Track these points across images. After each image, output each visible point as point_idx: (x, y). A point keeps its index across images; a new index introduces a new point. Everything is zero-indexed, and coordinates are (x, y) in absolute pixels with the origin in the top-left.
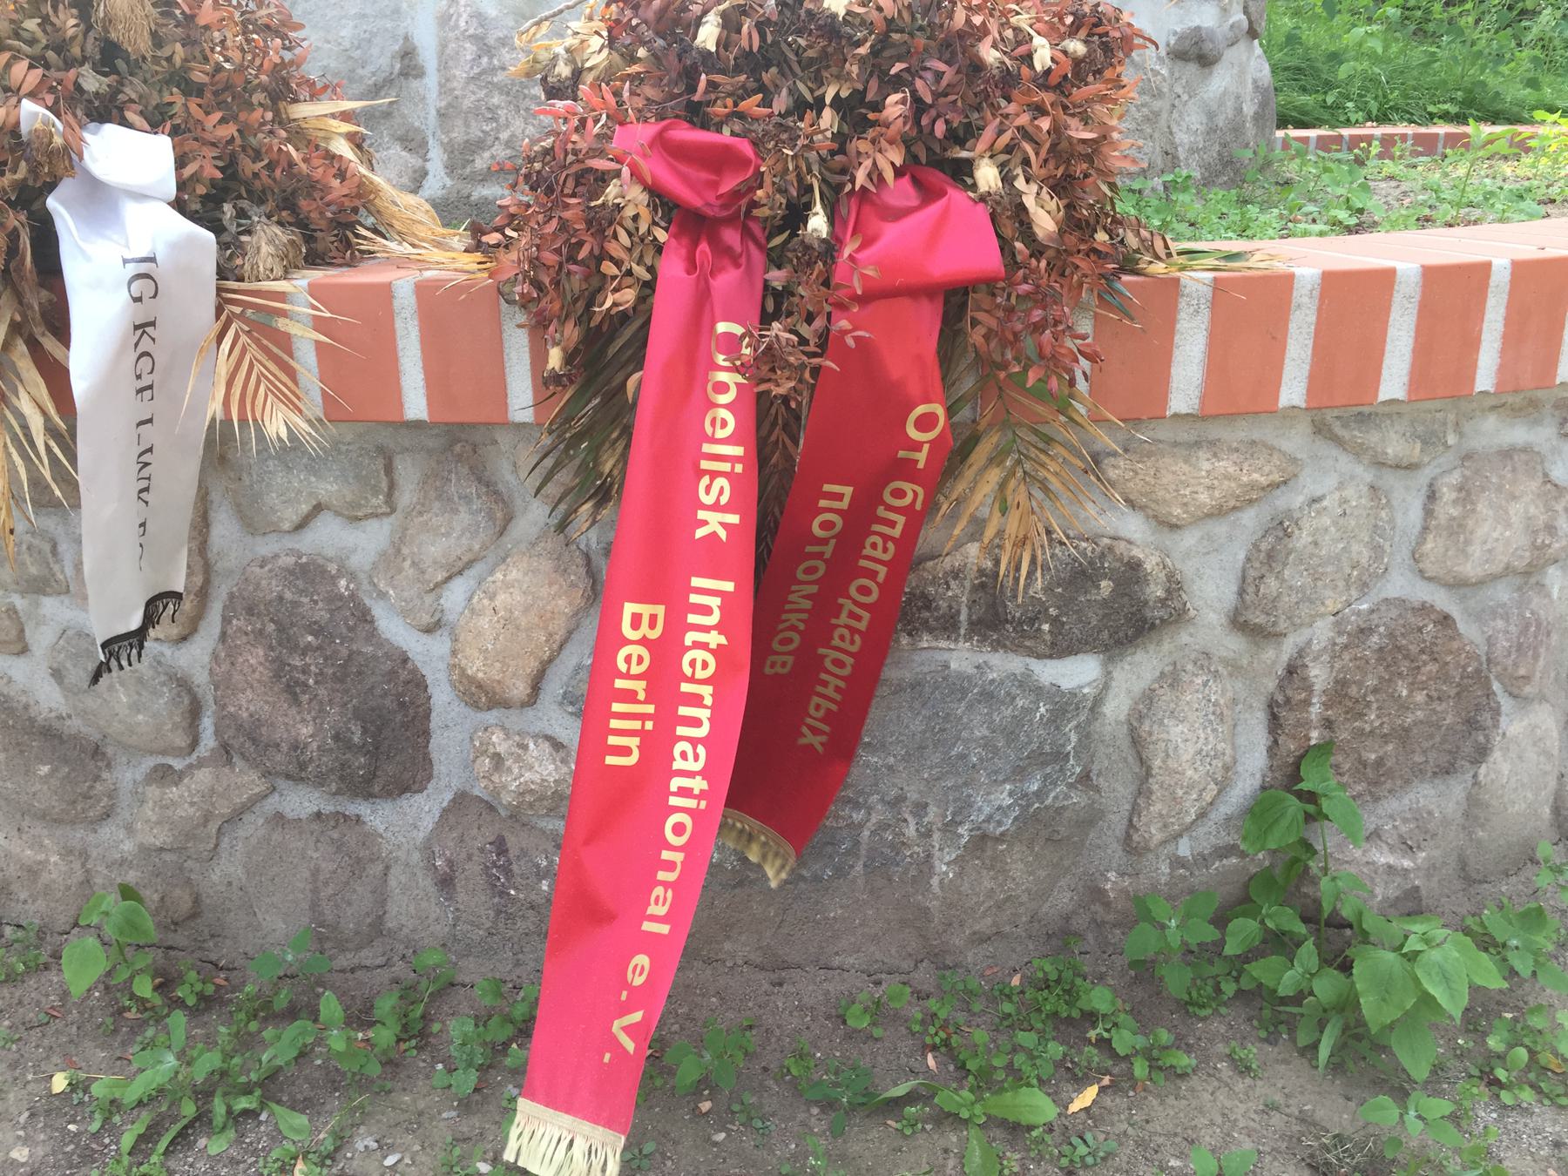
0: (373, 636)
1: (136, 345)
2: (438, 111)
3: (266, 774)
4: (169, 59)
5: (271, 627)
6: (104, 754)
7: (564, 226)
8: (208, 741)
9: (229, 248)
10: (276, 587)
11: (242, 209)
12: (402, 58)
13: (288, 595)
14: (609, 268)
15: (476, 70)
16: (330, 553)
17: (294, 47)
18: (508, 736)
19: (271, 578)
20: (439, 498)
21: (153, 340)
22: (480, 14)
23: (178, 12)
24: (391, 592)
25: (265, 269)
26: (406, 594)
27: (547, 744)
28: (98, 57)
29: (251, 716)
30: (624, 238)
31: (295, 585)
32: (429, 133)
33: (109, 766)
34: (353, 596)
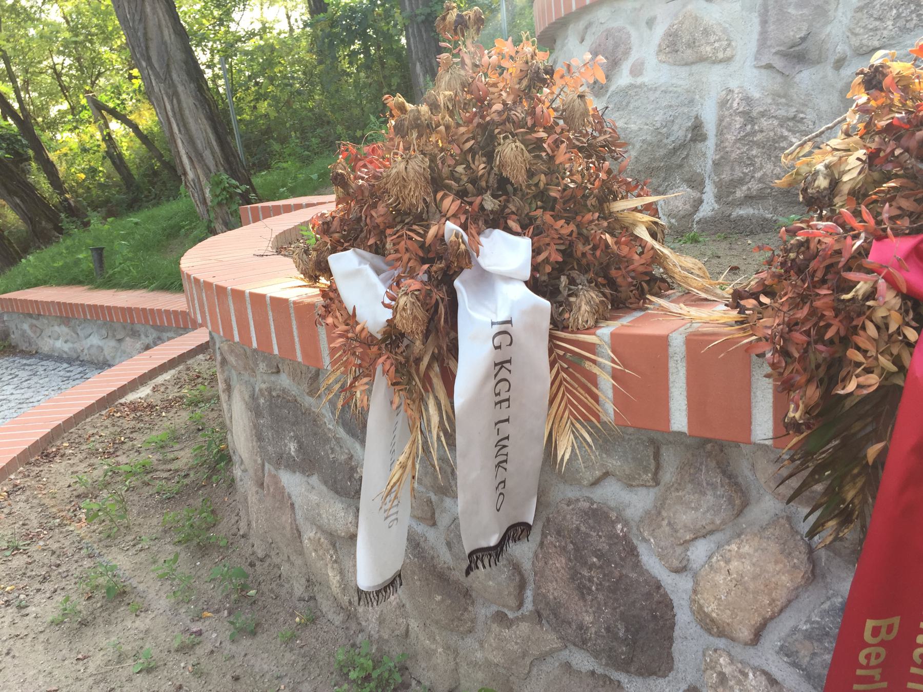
0: (637, 566)
1: (496, 376)
2: (713, 162)
3: (561, 638)
4: (537, 185)
5: (571, 547)
6: (470, 596)
7: (813, 312)
8: (529, 606)
9: (561, 306)
10: (576, 522)
11: (573, 278)
12: (693, 130)
13: (583, 528)
14: (854, 355)
15: (742, 134)
16: (612, 504)
17: (619, 158)
18: (732, 661)
19: (573, 514)
20: (691, 481)
21: (510, 371)
22: (748, 98)
23: (544, 154)
24: (652, 540)
25: (583, 322)
26: (662, 544)
27: (764, 678)
28: (496, 186)
29: (555, 599)
30: (872, 330)
31: (588, 523)
32: (706, 176)
33: (473, 603)
34: (625, 536)
